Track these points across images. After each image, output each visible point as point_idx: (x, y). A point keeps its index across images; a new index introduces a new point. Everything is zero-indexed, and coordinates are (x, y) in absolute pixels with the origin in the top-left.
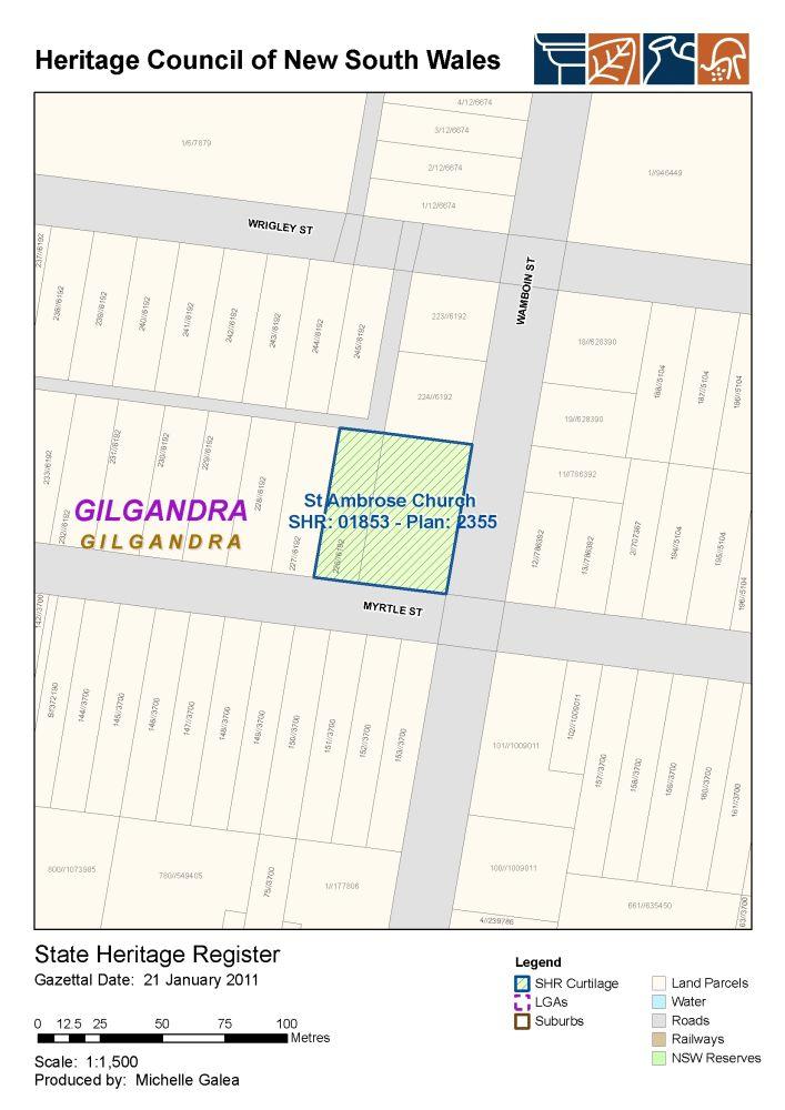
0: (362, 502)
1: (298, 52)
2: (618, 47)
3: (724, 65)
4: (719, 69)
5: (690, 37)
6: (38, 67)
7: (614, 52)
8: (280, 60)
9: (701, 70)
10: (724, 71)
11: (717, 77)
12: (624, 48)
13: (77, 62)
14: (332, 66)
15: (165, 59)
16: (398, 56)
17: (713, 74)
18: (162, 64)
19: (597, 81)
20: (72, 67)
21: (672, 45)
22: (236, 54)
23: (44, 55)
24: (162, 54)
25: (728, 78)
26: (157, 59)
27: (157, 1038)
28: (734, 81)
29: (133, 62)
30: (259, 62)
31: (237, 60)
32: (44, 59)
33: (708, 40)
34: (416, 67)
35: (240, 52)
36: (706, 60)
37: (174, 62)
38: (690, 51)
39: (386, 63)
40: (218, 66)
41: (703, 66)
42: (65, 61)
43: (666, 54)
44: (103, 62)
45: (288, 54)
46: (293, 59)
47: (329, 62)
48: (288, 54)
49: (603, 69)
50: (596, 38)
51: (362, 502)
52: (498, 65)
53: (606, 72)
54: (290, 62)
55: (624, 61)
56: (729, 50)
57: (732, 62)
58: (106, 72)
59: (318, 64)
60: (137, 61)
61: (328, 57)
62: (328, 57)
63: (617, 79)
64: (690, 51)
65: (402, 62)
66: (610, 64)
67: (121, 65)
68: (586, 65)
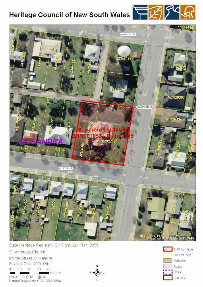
0: (95, 130)
1: (77, 13)
2: (157, 9)
3: (188, 14)
4: (187, 15)
5: (178, 6)
6: (10, 17)
7: (156, 10)
8: (72, 15)
9: (181, 16)
10: (188, 16)
11: (186, 17)
12: (159, 9)
13: (20, 15)
14: (86, 17)
15: (43, 15)
16: (103, 14)
17: (185, 17)
18: (42, 16)
19: (151, 19)
20: (19, 17)
21: (173, 8)
22: (61, 13)
23: (12, 14)
24: (42, 13)
25: (189, 17)
26: (41, 15)
27: (48, 273)
28: (191, 18)
29: (34, 15)
30: (67, 15)
31: (61, 15)
32: (12, 15)
33: (184, 7)
34: (108, 17)
35: (62, 13)
36: (183, 12)
37: (45, 15)
38: (178, 10)
39: (100, 16)
40: (56, 16)
41: (182, 14)
42: (17, 15)
43: (171, 11)
44: (27, 15)
45: (75, 13)
46: (77, 15)
47: (85, 15)
48: (75, 13)
49: (152, 15)
50: (151, 6)
51: (95, 130)
52: (129, 16)
53: (154, 16)
54: (75, 15)
55: (159, 13)
56: (190, 9)
57: (191, 13)
58: (27, 18)
59: (82, 16)
60: (35, 15)
61: (85, 14)
62: (85, 14)
63: (157, 18)
64: (178, 10)
65: (104, 16)
66: (155, 14)
67: (31, 16)
68: (148, 14)
